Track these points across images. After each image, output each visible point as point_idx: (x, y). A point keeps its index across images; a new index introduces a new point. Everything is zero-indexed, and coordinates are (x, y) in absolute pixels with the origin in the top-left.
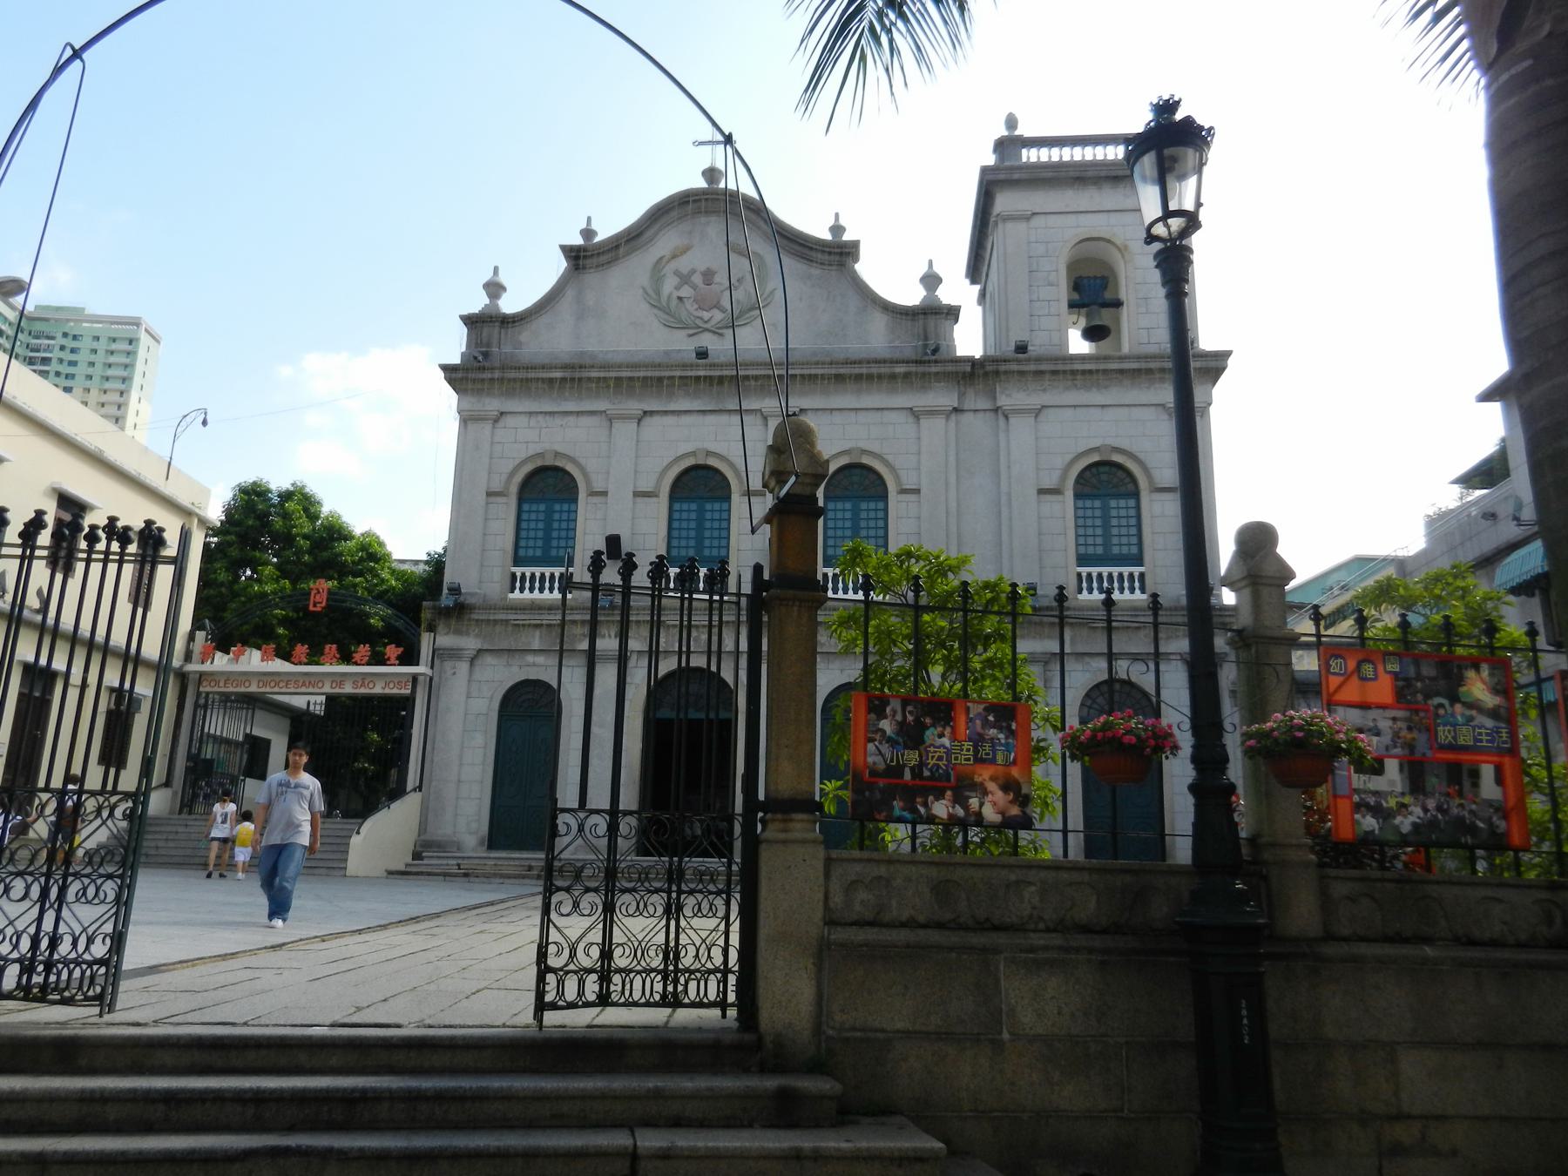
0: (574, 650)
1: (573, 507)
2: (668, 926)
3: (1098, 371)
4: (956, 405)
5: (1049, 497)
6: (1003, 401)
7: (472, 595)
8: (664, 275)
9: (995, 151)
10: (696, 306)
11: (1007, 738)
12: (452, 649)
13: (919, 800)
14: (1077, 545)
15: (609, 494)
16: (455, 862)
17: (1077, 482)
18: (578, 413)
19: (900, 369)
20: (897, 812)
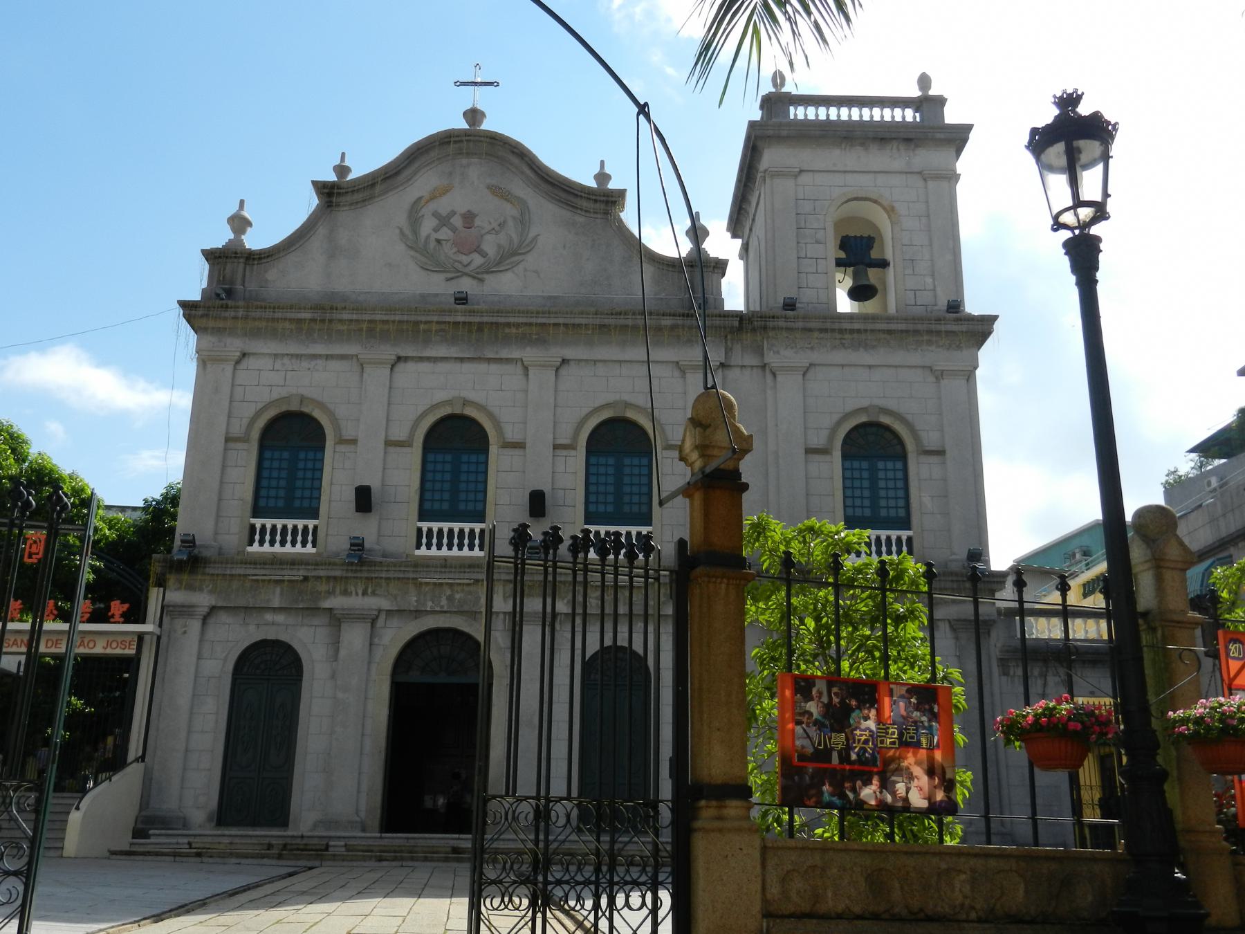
0: (319, 608)
1: (319, 456)
2: (534, 920)
3: (866, 331)
4: (723, 361)
5: (817, 457)
6: (771, 358)
7: (206, 547)
8: (423, 216)
9: (762, 107)
10: (455, 250)
11: (930, 721)
12: (183, 606)
13: (847, 785)
14: (845, 506)
15: (359, 443)
16: (185, 840)
17: (845, 442)
18: (328, 357)
19: (667, 322)
20: (826, 797)
